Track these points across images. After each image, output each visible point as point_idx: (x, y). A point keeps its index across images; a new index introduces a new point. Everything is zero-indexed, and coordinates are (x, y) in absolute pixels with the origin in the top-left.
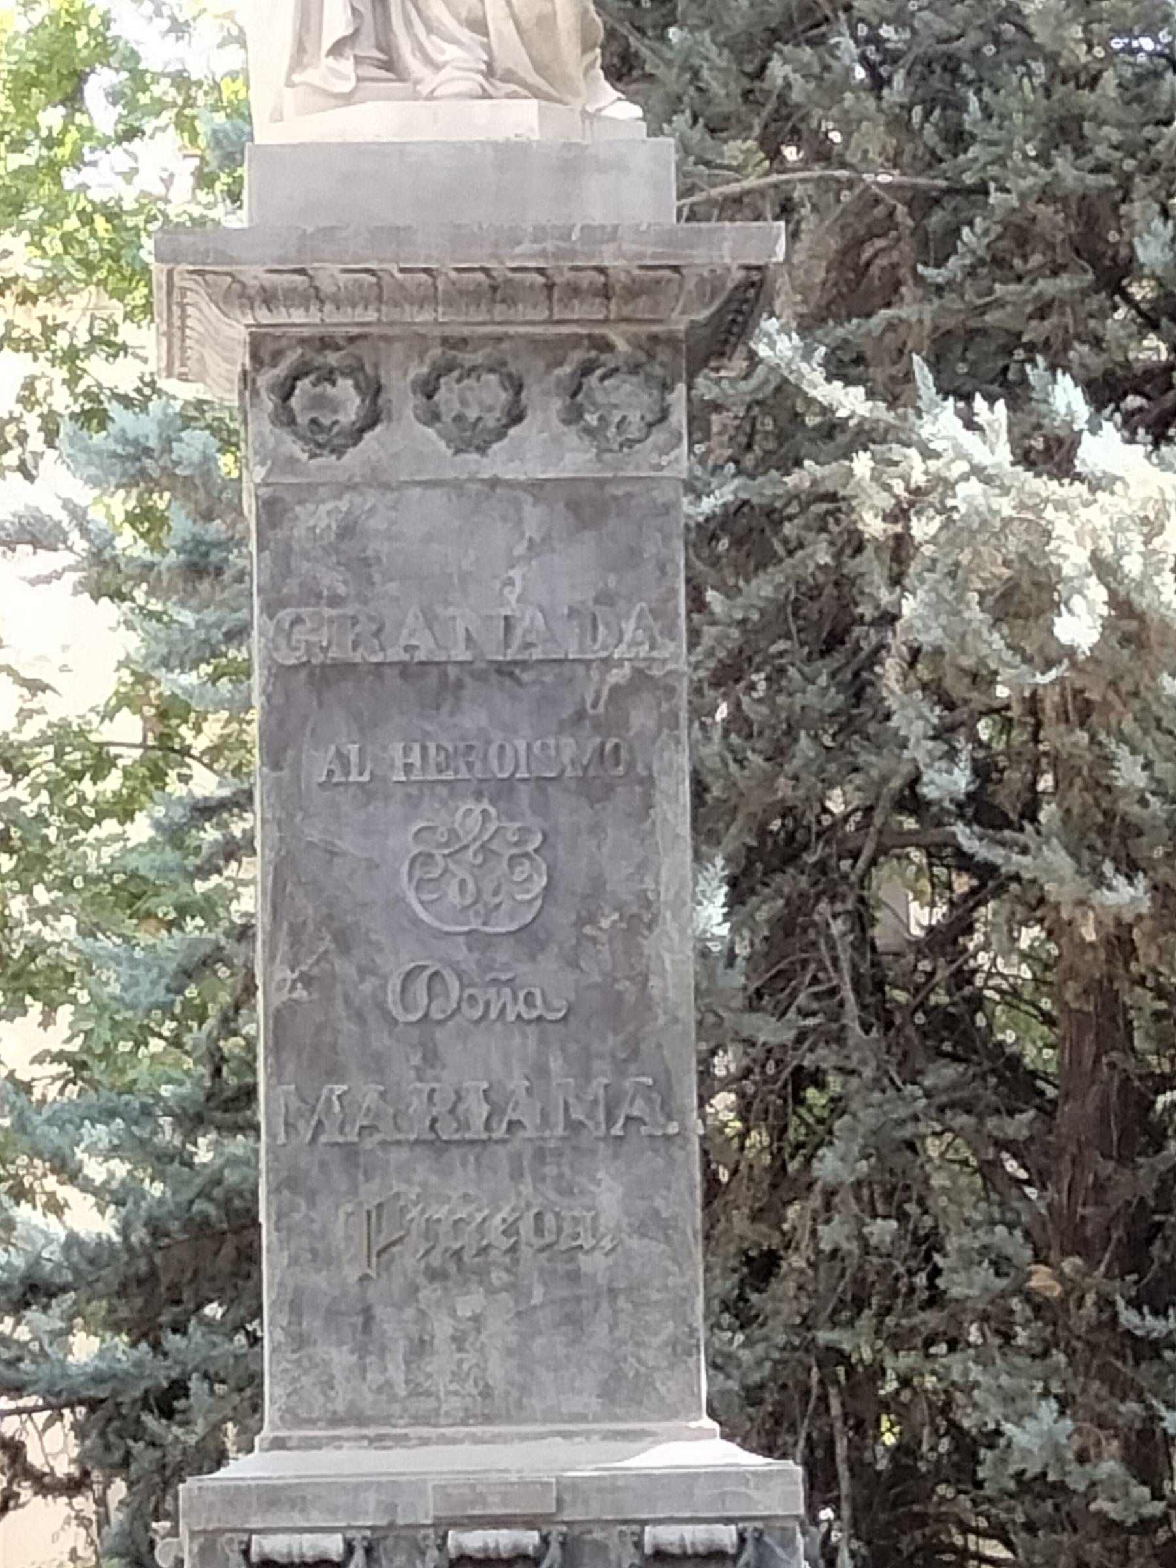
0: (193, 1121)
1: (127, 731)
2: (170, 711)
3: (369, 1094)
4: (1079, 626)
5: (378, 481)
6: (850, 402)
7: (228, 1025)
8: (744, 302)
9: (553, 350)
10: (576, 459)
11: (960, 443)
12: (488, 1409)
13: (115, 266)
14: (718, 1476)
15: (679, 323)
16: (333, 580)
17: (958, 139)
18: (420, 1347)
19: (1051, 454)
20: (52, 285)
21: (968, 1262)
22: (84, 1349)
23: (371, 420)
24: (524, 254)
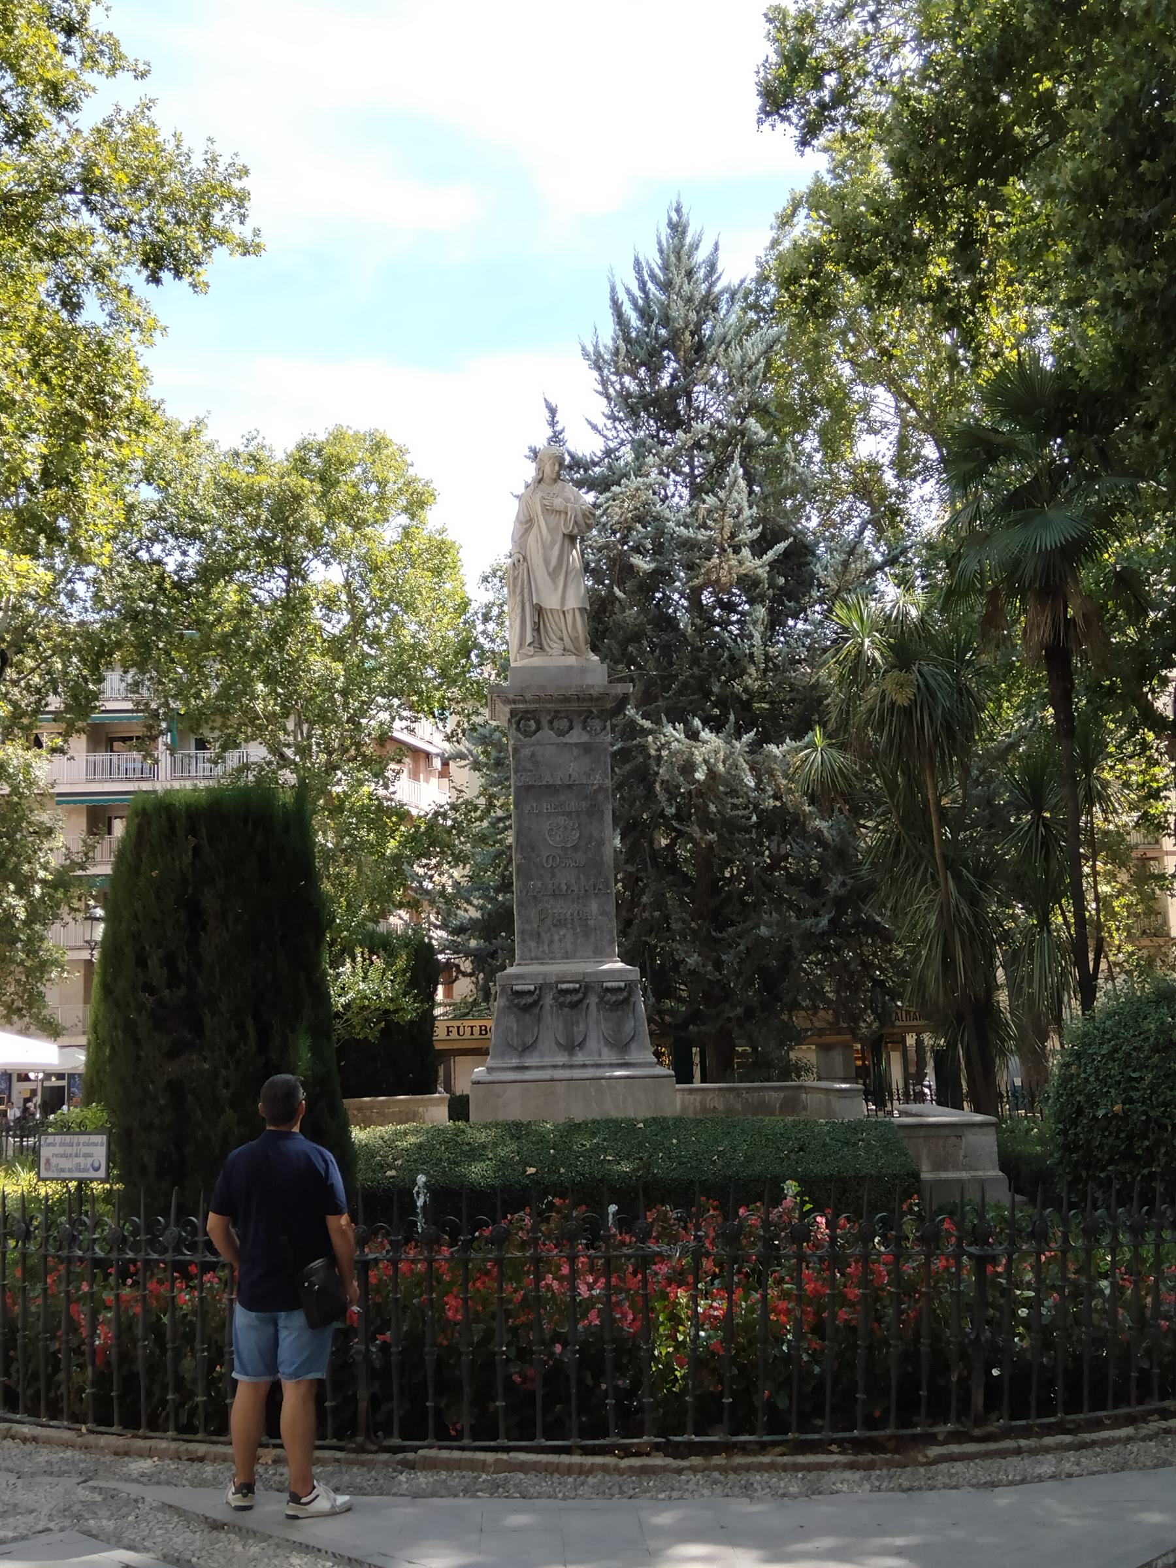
0: (498, 890)
1: (482, 801)
2: (491, 797)
3: (539, 884)
4: (700, 775)
5: (539, 743)
6: (647, 724)
7: (506, 868)
8: (623, 701)
9: (580, 713)
10: (585, 738)
11: (674, 733)
12: (567, 956)
13: (478, 695)
14: (619, 971)
15: (608, 707)
16: (529, 766)
17: (671, 664)
18: (551, 942)
19: (693, 735)
20: (464, 700)
21: (677, 921)
22: (473, 943)
23: (538, 729)
24: (572, 691)
